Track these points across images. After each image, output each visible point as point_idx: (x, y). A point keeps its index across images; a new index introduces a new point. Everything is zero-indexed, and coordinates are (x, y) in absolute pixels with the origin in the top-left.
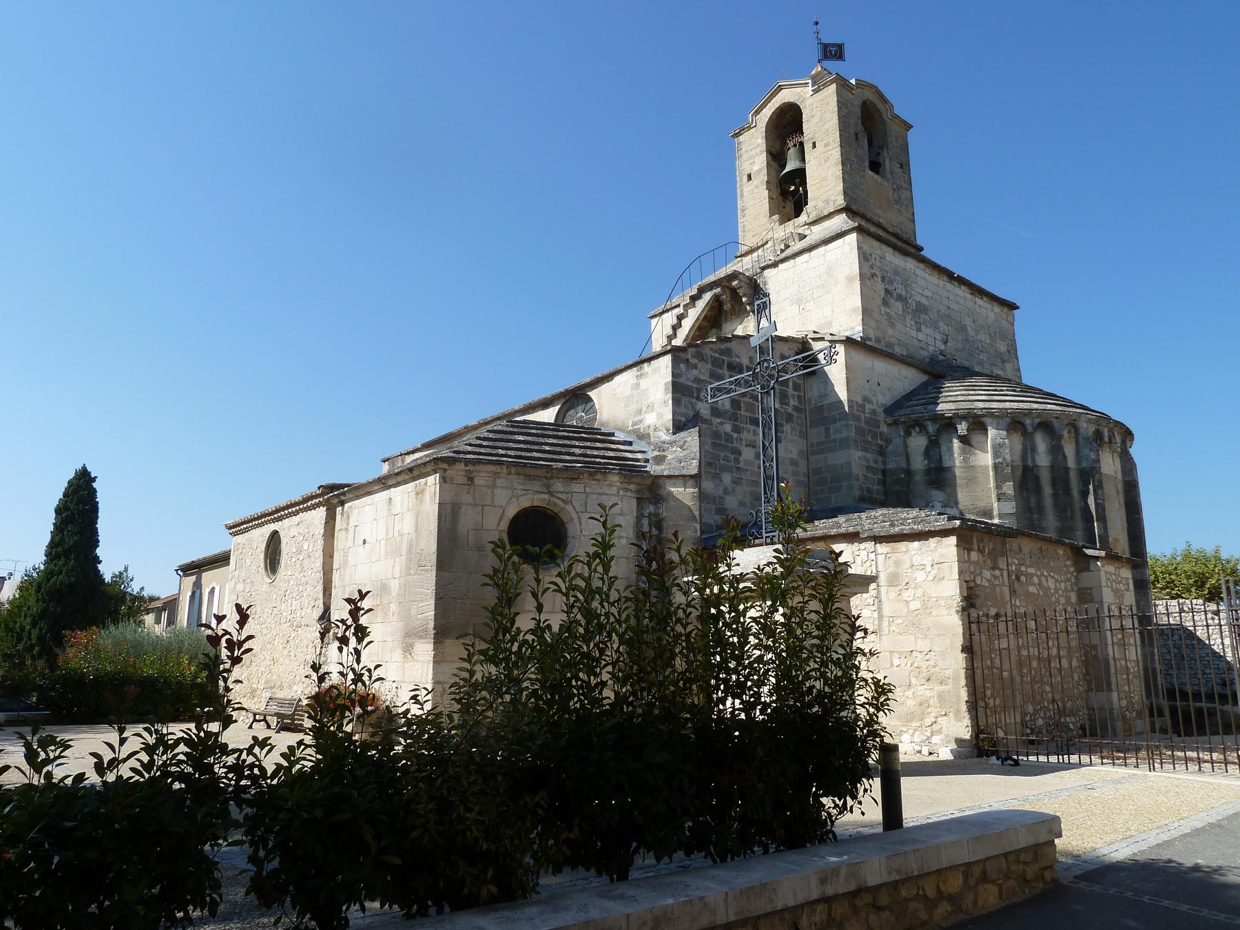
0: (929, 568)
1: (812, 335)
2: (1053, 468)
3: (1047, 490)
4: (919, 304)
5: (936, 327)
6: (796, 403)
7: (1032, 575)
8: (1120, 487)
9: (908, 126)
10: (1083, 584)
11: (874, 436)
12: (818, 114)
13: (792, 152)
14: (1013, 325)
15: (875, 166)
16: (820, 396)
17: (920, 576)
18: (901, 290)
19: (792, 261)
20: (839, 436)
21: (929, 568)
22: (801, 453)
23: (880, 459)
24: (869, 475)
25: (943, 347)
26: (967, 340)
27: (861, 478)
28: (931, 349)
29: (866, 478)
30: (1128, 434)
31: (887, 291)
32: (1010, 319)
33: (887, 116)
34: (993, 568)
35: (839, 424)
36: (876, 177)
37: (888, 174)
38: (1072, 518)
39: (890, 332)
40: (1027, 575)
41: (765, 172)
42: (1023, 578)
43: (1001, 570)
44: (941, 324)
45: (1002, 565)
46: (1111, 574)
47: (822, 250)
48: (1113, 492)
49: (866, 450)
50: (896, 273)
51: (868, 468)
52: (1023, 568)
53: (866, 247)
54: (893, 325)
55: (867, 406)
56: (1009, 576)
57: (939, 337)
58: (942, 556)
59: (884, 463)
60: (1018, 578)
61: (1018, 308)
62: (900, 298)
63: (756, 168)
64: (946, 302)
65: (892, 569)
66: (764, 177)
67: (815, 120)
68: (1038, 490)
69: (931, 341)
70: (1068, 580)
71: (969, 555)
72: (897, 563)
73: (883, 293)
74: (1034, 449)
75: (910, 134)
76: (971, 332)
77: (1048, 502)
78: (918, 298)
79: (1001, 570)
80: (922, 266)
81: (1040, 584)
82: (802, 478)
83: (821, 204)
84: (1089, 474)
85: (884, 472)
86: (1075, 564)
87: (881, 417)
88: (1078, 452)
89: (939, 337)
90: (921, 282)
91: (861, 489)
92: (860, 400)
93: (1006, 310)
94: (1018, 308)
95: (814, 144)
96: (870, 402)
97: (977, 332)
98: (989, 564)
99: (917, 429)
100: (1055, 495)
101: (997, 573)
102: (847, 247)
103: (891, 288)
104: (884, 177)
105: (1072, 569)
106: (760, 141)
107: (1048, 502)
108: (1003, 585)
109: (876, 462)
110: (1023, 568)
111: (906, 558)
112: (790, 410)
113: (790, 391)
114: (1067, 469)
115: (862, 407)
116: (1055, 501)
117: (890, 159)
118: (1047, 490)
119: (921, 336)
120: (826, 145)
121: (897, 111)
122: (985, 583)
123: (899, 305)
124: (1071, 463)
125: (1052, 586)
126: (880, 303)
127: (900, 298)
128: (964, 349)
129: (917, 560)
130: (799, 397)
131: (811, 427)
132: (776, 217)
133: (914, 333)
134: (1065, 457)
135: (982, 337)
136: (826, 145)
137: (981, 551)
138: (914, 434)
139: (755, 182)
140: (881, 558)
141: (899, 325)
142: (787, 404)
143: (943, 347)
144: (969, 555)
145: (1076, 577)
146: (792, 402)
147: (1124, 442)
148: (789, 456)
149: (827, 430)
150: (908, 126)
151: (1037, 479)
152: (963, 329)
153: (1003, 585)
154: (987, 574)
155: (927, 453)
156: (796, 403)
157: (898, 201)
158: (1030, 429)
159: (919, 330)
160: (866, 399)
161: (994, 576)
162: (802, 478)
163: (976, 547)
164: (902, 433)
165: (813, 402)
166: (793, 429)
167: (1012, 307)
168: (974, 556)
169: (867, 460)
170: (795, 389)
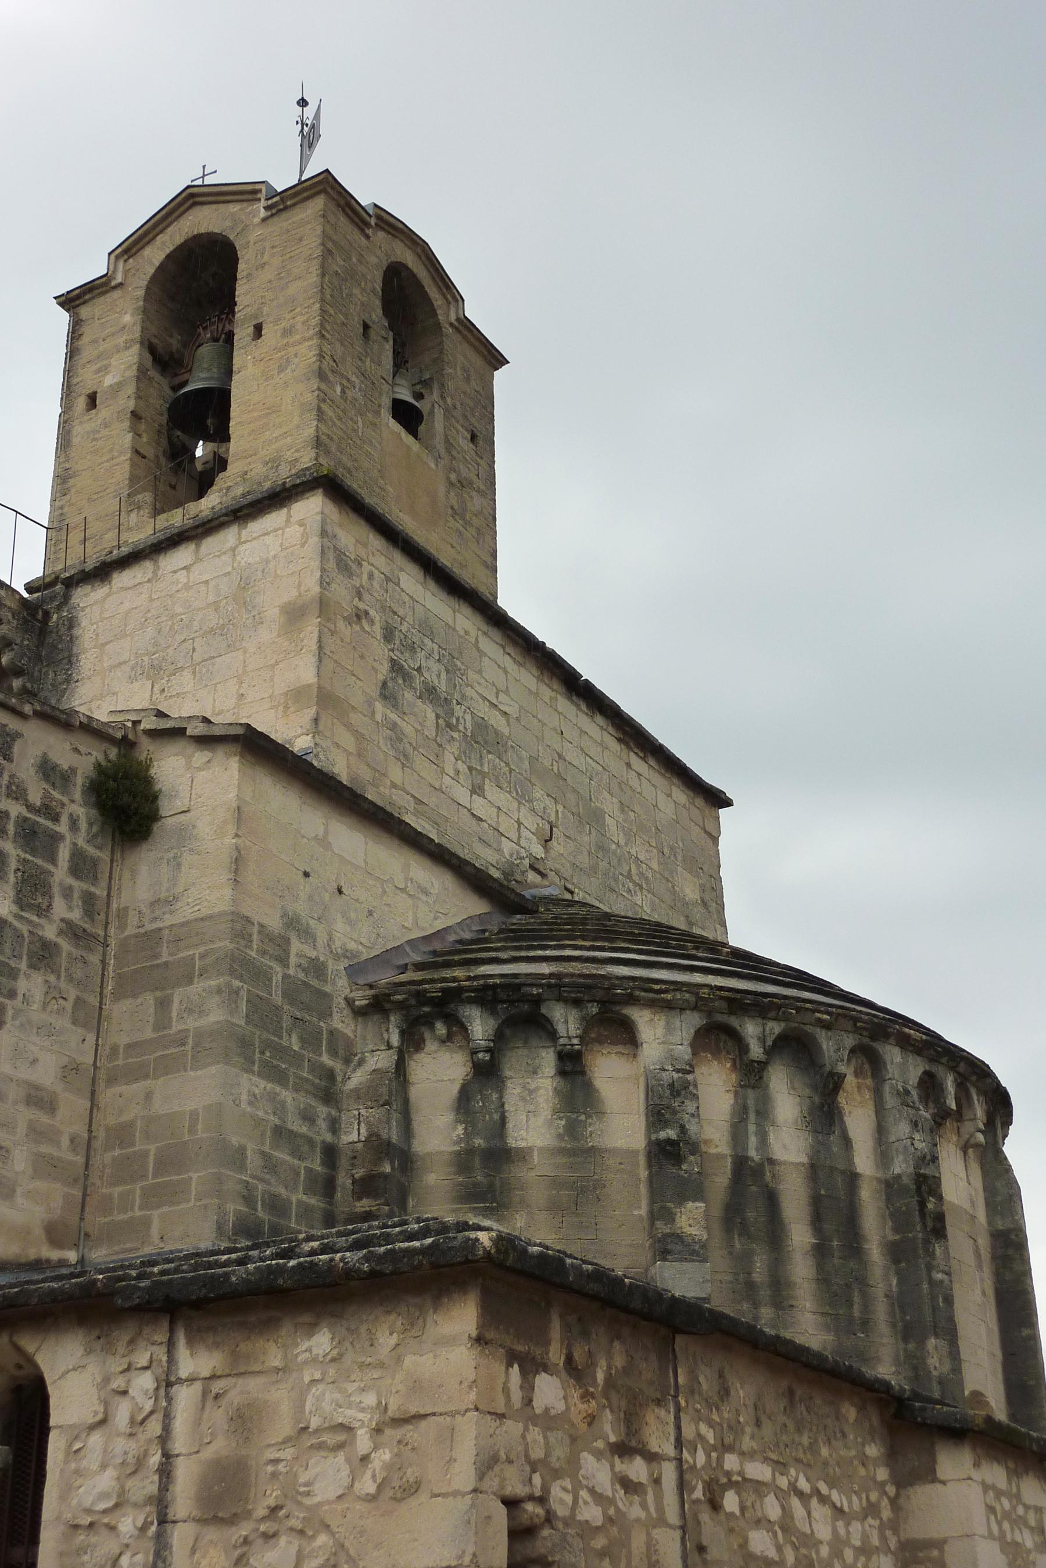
0: (363, 1442)
1: (149, 723)
2: (814, 1170)
3: (800, 1235)
4: (481, 725)
5: (523, 798)
6: (76, 915)
7: (759, 1487)
8: (984, 1242)
9: (497, 360)
10: (916, 1529)
11: (311, 1040)
12: (276, 261)
13: (206, 351)
14: (715, 840)
15: (408, 416)
16: (154, 903)
17: (326, 1477)
18: (435, 674)
19: (148, 564)
20: (192, 1023)
21: (363, 1442)
22: (70, 1070)
23: (323, 1111)
24: (282, 1155)
25: (538, 851)
26: (601, 848)
27: (252, 1160)
28: (507, 847)
29: (270, 1165)
30: (1000, 1106)
31: (396, 667)
32: (710, 827)
33: (446, 316)
34: (623, 1450)
35: (199, 986)
36: (408, 438)
37: (439, 442)
38: (866, 1324)
39: (396, 773)
40: (743, 1485)
41: (130, 389)
42: (731, 1502)
43: (651, 1458)
44: (538, 793)
45: (660, 1441)
46: (999, 1494)
47: (229, 536)
48: (970, 1259)
49: (279, 1077)
50: (426, 628)
51: (280, 1133)
52: (731, 1462)
53: (326, 511)
54: (405, 760)
55: (296, 946)
56: (682, 1486)
57: (531, 822)
58: (416, 1386)
59: (334, 1126)
60: (715, 1505)
61: (728, 803)
62: (430, 693)
63: (109, 380)
64: (556, 743)
65: (220, 1447)
66: (126, 402)
67: (268, 274)
68: (775, 1234)
69: (507, 825)
70: (871, 1510)
71: (528, 1387)
72: (245, 1421)
73: (384, 668)
74: (764, 1113)
75: (500, 376)
76: (613, 831)
77: (801, 1269)
78: (483, 710)
79: (651, 1458)
80: (496, 634)
81: (786, 1525)
82: (64, 1152)
83: (258, 470)
84: (918, 1200)
85: (330, 1153)
86: (892, 1456)
87: (340, 987)
88: (881, 1131)
89: (531, 822)
90: (492, 673)
91: (248, 1199)
92: (274, 923)
93: (700, 802)
94: (728, 803)
95: (258, 330)
96: (307, 935)
97: (629, 835)
98: (610, 1430)
99: (441, 1029)
100: (820, 1251)
101: (637, 1469)
102: (294, 532)
103: (409, 663)
104: (428, 447)
105: (882, 1474)
106: (127, 318)
107: (801, 1269)
108: (661, 1521)
109: (308, 1117)
110: (731, 1462)
111: (280, 1396)
112: (50, 932)
113: (60, 873)
114: (853, 1178)
115: (278, 946)
116: (820, 1266)
117: (448, 413)
118: (800, 1235)
119: (479, 806)
120: (288, 332)
121: (472, 312)
122: (591, 1513)
123: (429, 712)
124: (864, 1162)
125: (823, 1532)
126: (374, 691)
127: (430, 693)
128: (594, 869)
129: (325, 1403)
130: (89, 900)
131: (119, 995)
132: (147, 497)
133: (462, 794)
134: (847, 1142)
135: (639, 850)
136: (288, 332)
137: (576, 1372)
138: (431, 1046)
139: (103, 412)
140: (185, 1398)
141: (421, 764)
142: (44, 911)
143: (538, 851)
144: (528, 1387)
145: (894, 1502)
146: (59, 908)
147: (990, 1123)
148: (25, 1073)
149: (163, 1004)
150: (497, 360)
151: (772, 1200)
152: (595, 818)
153: (661, 1521)
154: (598, 1472)
155: (464, 1102)
156: (76, 915)
157: (458, 513)
158: (756, 1051)
159: (477, 790)
160: (292, 922)
161: (628, 1485)
162: (64, 1152)
163: (556, 1354)
164: (395, 1039)
165: (133, 919)
166: (53, 994)
167: (718, 800)
168: (549, 1391)
169: (280, 1108)
170: (75, 870)
